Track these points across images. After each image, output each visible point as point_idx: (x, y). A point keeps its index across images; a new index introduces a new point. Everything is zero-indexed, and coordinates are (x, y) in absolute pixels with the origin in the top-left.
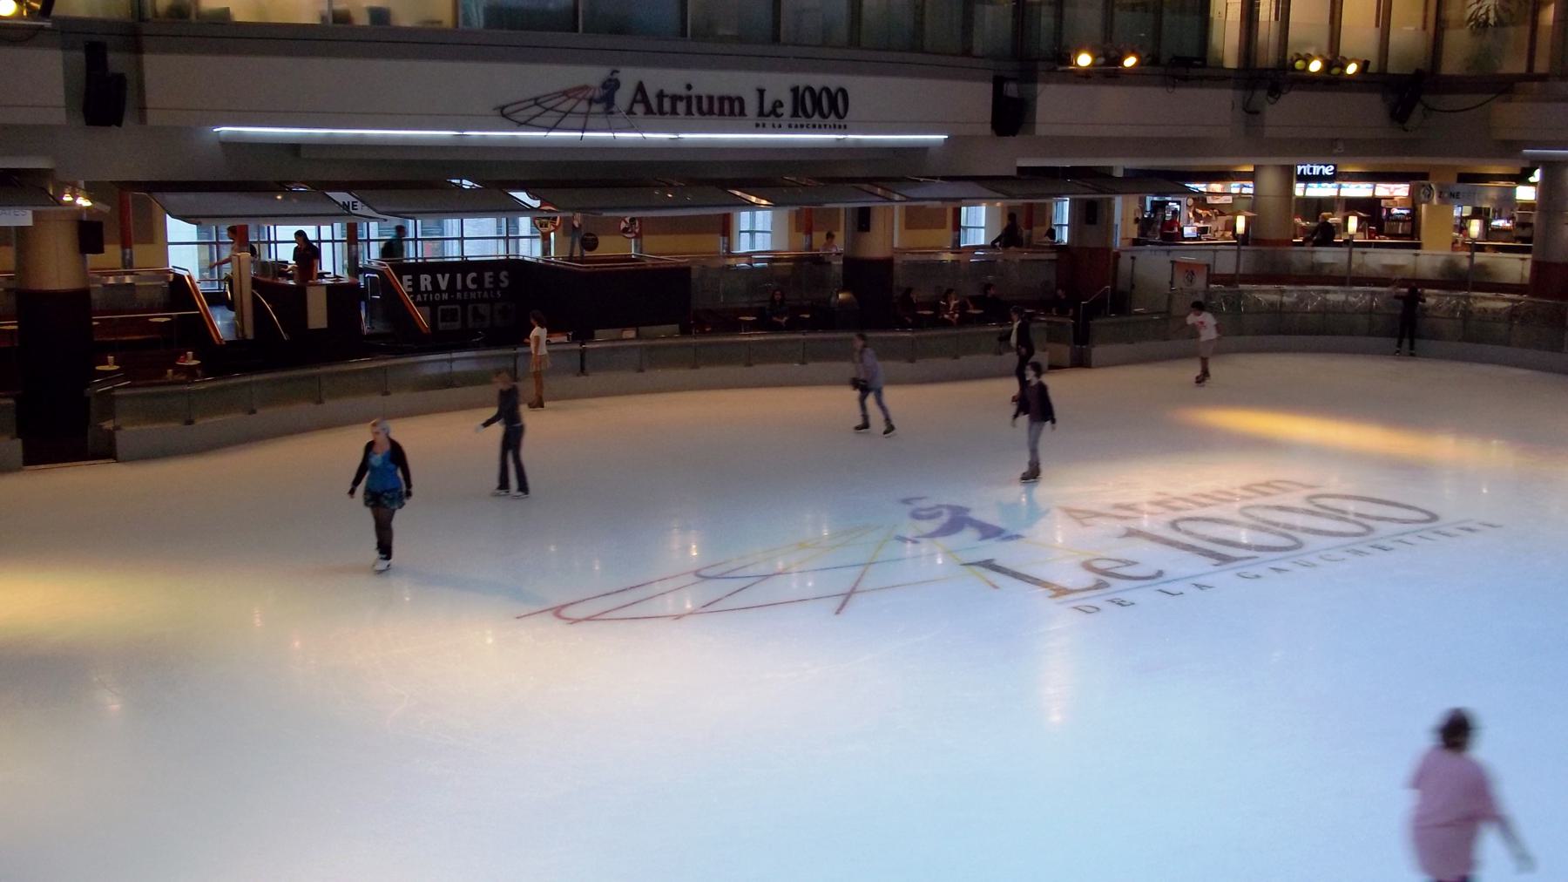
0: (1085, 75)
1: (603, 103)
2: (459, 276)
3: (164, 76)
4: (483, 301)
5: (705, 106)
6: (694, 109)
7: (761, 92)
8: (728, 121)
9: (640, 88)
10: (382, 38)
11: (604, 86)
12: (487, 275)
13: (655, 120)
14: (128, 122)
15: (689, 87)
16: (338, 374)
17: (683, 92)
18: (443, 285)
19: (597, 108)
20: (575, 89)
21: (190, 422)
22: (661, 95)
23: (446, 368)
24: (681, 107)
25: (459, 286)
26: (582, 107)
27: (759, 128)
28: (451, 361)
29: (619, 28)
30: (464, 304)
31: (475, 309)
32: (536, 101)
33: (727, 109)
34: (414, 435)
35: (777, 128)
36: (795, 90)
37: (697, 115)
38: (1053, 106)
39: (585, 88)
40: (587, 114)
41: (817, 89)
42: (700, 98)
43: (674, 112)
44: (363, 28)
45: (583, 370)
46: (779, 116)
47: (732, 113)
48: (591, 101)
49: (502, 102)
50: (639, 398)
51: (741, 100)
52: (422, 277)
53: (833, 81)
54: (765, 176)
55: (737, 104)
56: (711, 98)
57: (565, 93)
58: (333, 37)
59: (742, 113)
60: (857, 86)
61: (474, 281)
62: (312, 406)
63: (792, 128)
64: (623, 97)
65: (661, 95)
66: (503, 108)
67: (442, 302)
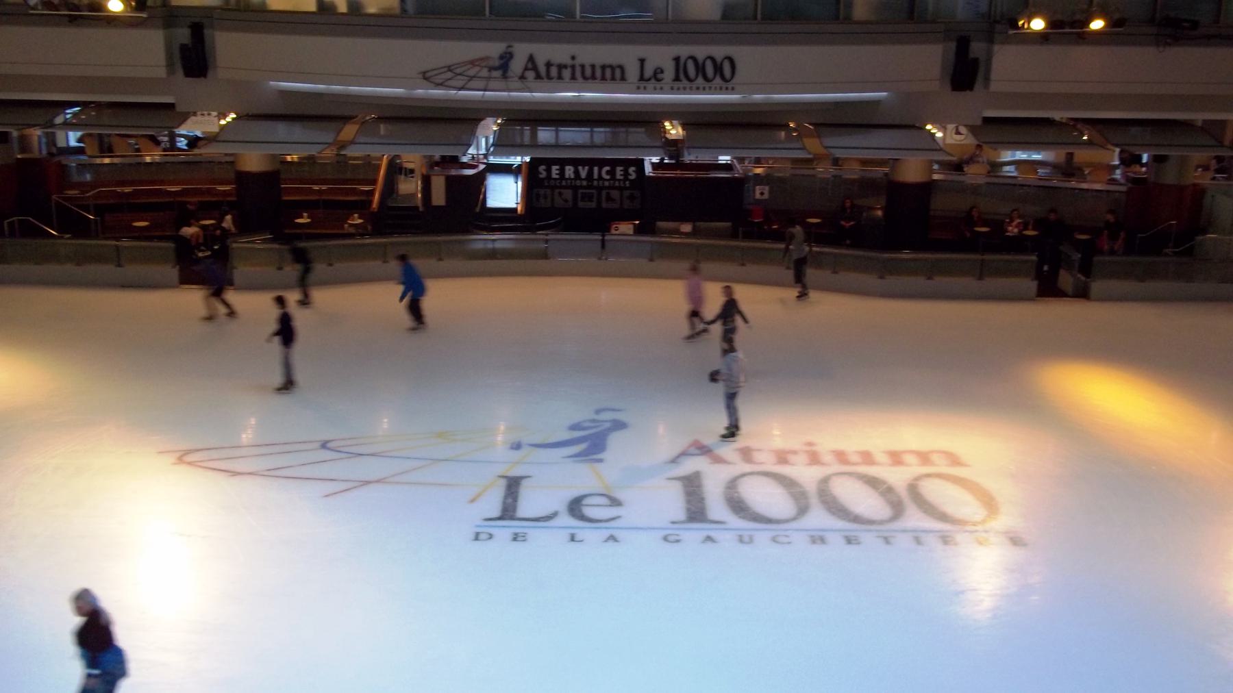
0: (1042, 37)
2: (596, 169)
3: (227, 46)
4: (613, 188)
5: (588, 72)
6: (578, 74)
7: (642, 61)
9: (531, 58)
10: (357, 22)
11: (501, 57)
13: (539, 83)
14: (978, 85)
15: (573, 58)
16: (451, 241)
17: (569, 62)
18: (583, 174)
20: (482, 59)
21: (331, 265)
22: (549, 65)
24: (567, 73)
25: (596, 176)
26: (485, 73)
29: (535, 14)
30: (600, 189)
31: (560, 194)
33: (611, 74)
34: (743, 294)
35: (662, 90)
36: (677, 59)
37: (580, 79)
38: (1008, 67)
40: (489, 78)
41: (700, 57)
42: (583, 66)
43: (560, 77)
44: (342, 14)
46: (659, 80)
47: (613, 79)
48: (491, 69)
49: (423, 70)
51: (621, 68)
52: (567, 168)
53: (719, 52)
55: (618, 72)
56: (593, 66)
58: (322, 20)
59: (623, 79)
60: (742, 53)
61: (608, 173)
62: (379, 263)
64: (517, 65)
65: (549, 65)
66: (424, 73)
67: (581, 187)
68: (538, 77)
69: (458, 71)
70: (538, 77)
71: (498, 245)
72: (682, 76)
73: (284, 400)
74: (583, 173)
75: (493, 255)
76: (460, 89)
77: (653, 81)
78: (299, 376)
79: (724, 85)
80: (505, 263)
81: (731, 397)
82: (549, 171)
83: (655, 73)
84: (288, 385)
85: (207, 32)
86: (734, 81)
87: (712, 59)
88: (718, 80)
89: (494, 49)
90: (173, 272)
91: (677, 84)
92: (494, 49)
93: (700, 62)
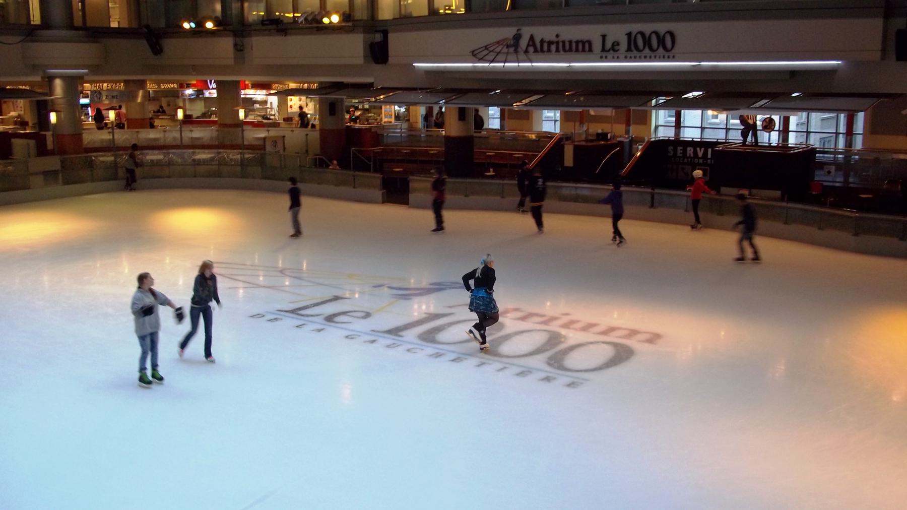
1: (514, 48)
3: (397, 42)
7: (604, 37)
8: (578, 55)
9: (532, 38)
12: (680, 148)
13: (540, 55)
17: (554, 39)
18: (700, 154)
19: (512, 50)
22: (542, 41)
23: (573, 192)
24: (553, 48)
26: (505, 50)
27: (602, 59)
28: (576, 188)
31: (683, 169)
32: (486, 48)
33: (582, 48)
35: (618, 59)
36: (629, 35)
37: (562, 52)
39: (506, 39)
42: (564, 42)
43: (549, 50)
45: (652, 206)
46: (615, 51)
47: (584, 50)
49: (472, 49)
50: (679, 227)
51: (590, 43)
52: (689, 149)
53: (662, 27)
54: (550, 91)
55: (587, 45)
56: (570, 42)
57: (498, 42)
59: (590, 50)
60: (682, 29)
63: (626, 59)
64: (524, 43)
68: (536, 51)
69: (491, 49)
70: (536, 51)
71: (579, 192)
72: (633, 48)
73: (297, 241)
74: (700, 153)
75: (576, 199)
76: (492, 62)
77: (611, 52)
78: (304, 229)
79: (667, 54)
80: (572, 205)
81: (295, 204)
82: (675, 150)
83: (613, 45)
84: (297, 233)
85: (389, 35)
86: (673, 51)
87: (656, 33)
88: (661, 50)
89: (508, 32)
90: (378, 194)
91: (629, 54)
92: (508, 32)
93: (647, 36)
